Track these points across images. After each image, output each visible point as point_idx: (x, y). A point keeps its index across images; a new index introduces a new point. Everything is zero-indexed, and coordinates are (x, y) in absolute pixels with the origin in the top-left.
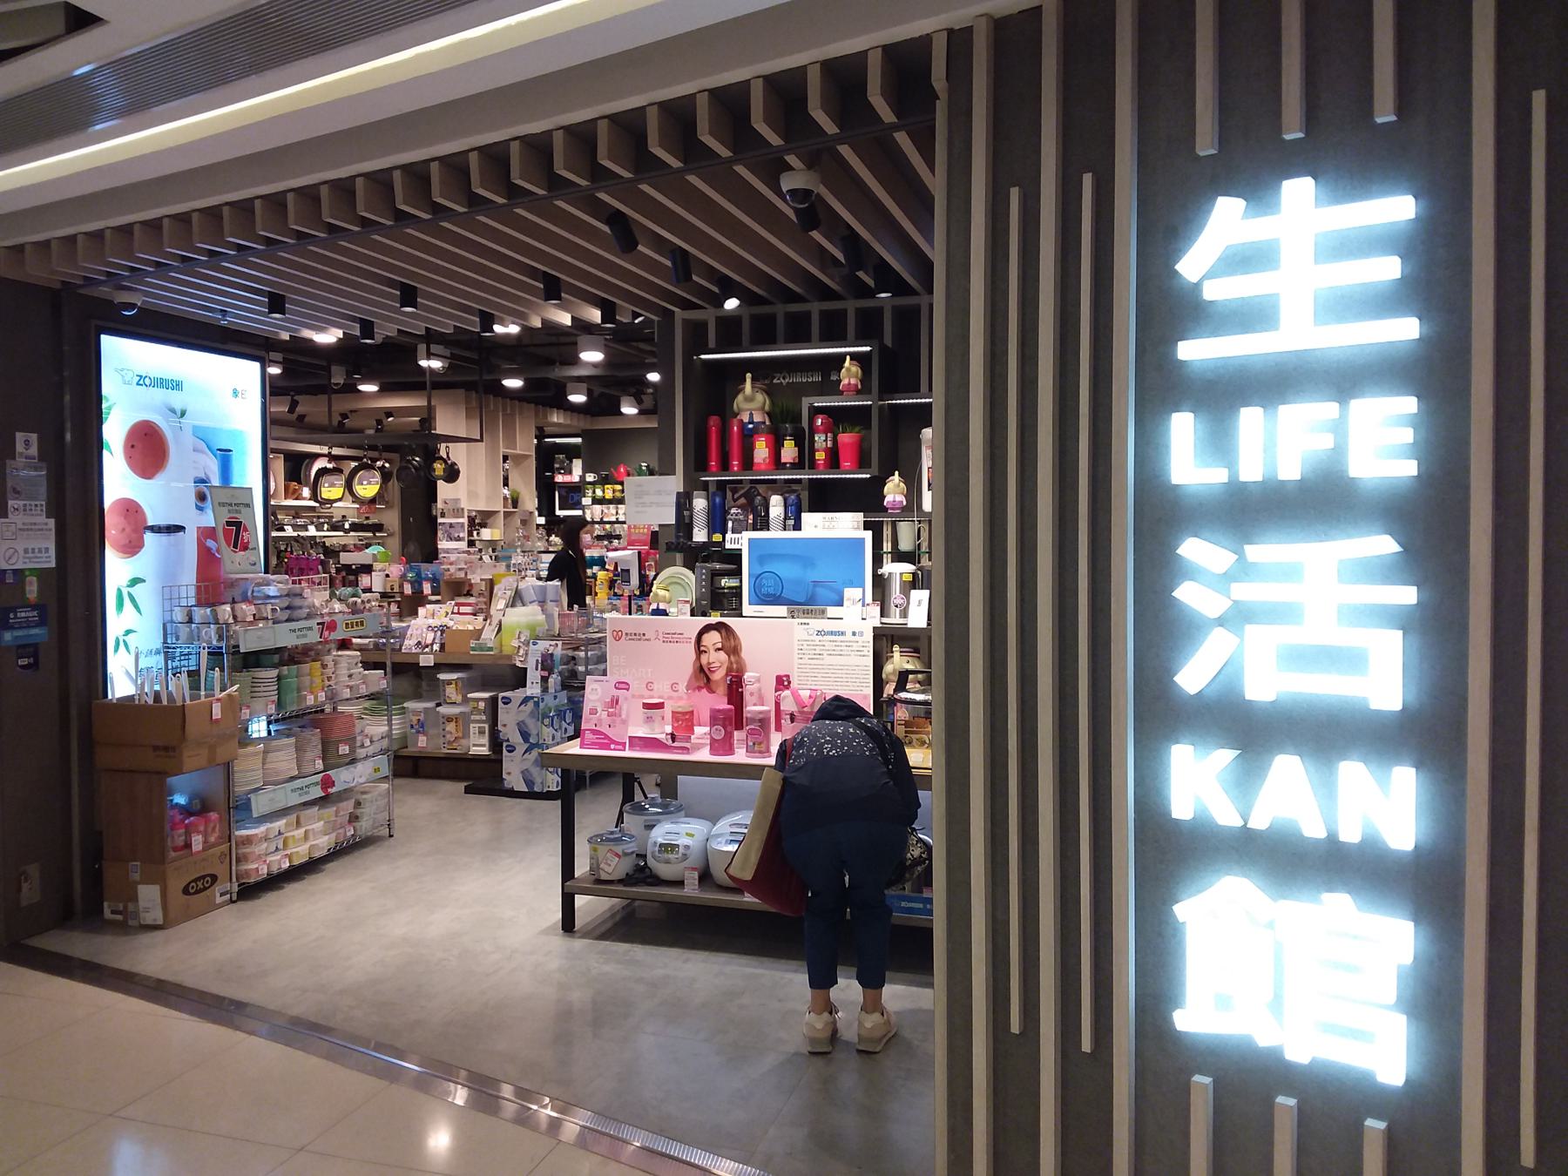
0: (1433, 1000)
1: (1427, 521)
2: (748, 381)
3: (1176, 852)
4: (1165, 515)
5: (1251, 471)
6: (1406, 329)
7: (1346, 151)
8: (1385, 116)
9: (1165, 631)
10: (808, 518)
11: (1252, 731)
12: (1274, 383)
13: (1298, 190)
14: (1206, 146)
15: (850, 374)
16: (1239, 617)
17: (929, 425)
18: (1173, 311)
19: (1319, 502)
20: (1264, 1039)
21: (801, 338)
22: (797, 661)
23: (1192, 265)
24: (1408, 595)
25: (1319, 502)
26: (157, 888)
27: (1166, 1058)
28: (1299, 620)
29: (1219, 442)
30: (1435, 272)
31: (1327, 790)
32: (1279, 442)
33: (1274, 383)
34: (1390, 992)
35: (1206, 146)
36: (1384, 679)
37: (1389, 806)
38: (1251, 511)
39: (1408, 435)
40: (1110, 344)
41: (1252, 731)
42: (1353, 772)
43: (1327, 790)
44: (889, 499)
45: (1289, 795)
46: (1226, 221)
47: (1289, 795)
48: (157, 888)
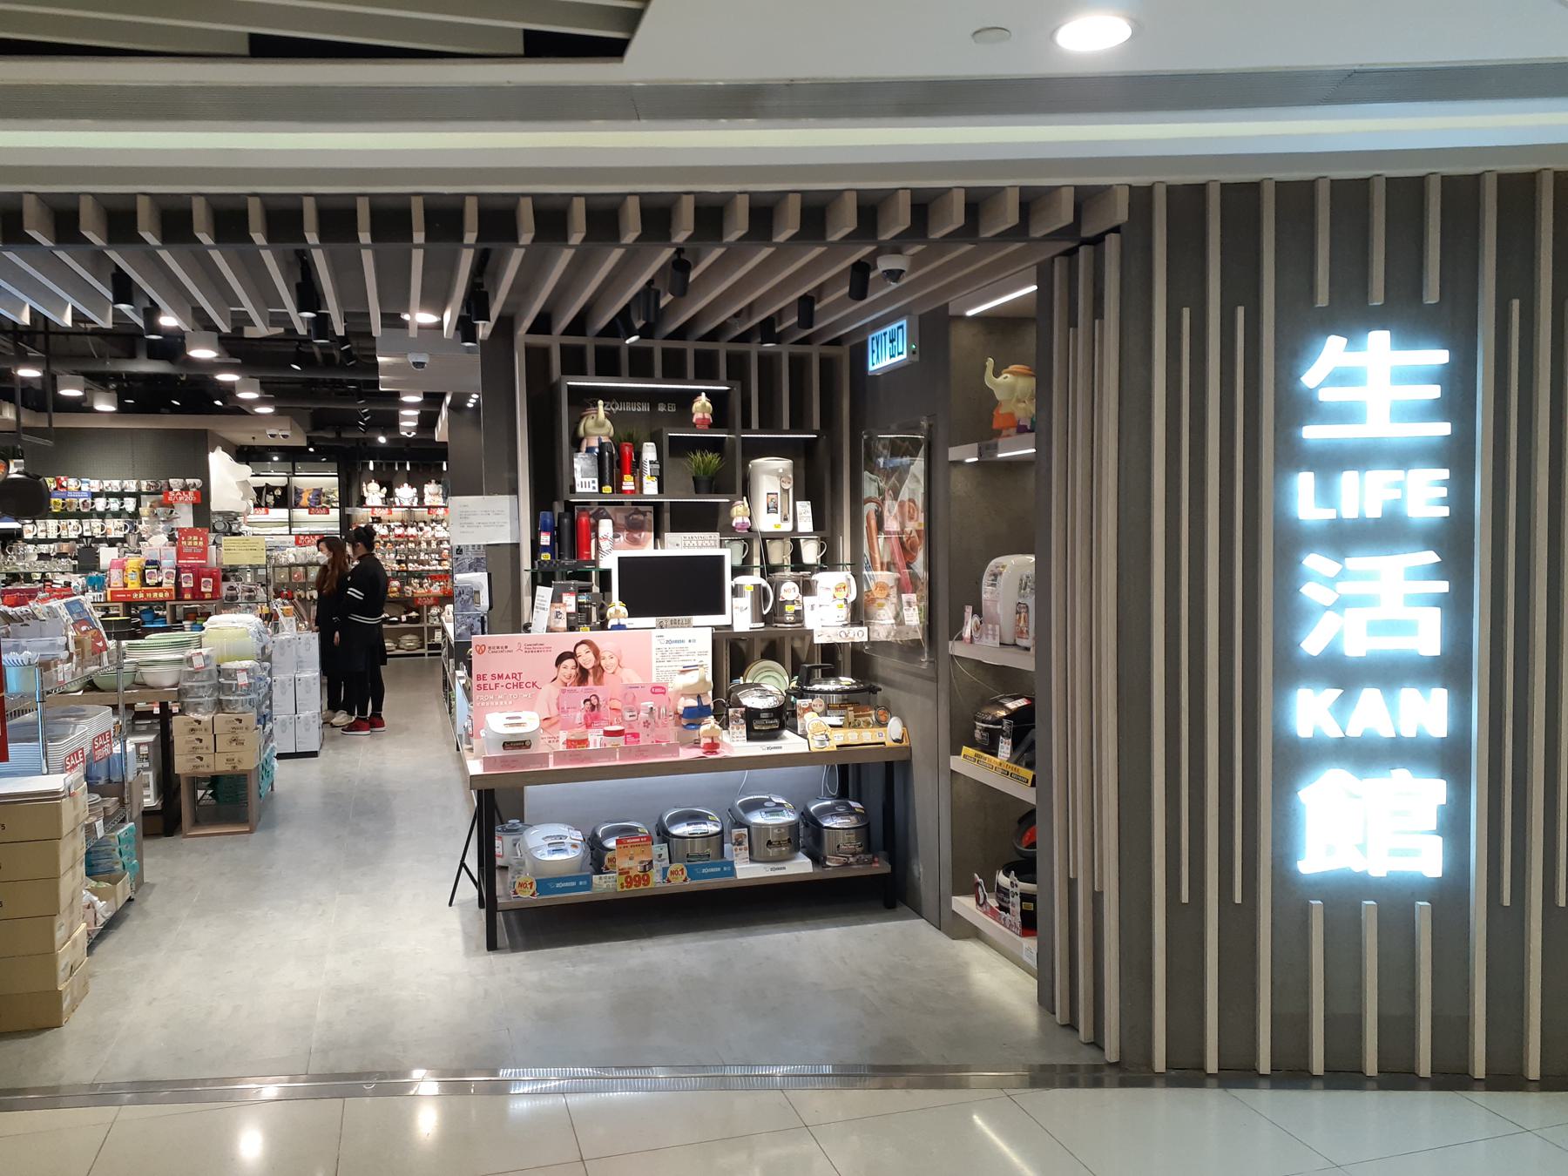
0: (1453, 825)
1: (1451, 541)
2: (601, 408)
3: (1298, 758)
4: (1293, 541)
5: (1349, 512)
6: (1444, 429)
7: (1408, 315)
8: (1432, 296)
9: (1291, 614)
10: (669, 537)
11: (1344, 675)
12: (1362, 457)
13: (1379, 339)
14: (1322, 300)
15: (702, 408)
16: (1341, 605)
17: (123, 409)
18: (1297, 407)
19: (1385, 533)
20: (1358, 867)
21: (647, 374)
22: (654, 664)
23: (1311, 377)
24: (1443, 587)
25: (1385, 533)
27: (1291, 891)
28: (1372, 602)
29: (1326, 494)
31: (1392, 708)
32: (1363, 495)
33: (1362, 457)
34: (1433, 824)
35: (1322, 300)
36: (1428, 639)
37: (1427, 712)
38: (1346, 537)
39: (1443, 492)
40: (1258, 429)
41: (1344, 675)
42: (1409, 695)
43: (1392, 708)
45: (1374, 715)
46: (1332, 352)
47: (1374, 715)
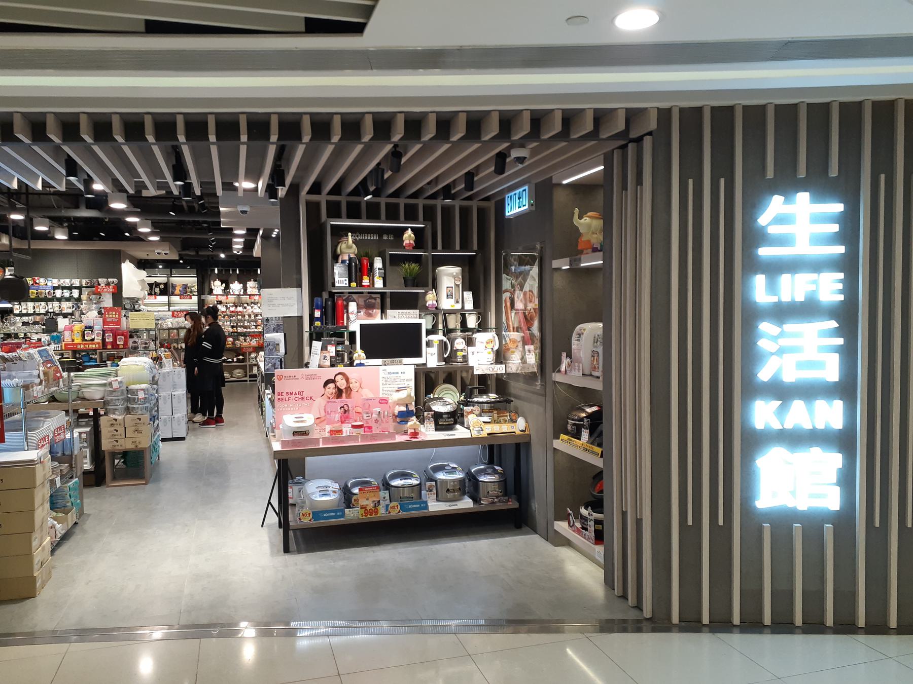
0: (846, 480)
1: (845, 315)
2: (350, 237)
3: (756, 441)
4: (753, 314)
5: (786, 298)
6: (841, 249)
7: (820, 183)
8: (834, 172)
9: (752, 357)
10: (390, 312)
11: (783, 392)
12: (793, 266)
13: (803, 197)
14: (770, 174)
15: (408, 237)
16: (781, 352)
17: (71, 238)
18: (755, 237)
19: (807, 310)
20: (790, 504)
21: (377, 218)
22: (381, 386)
23: (763, 219)
24: (840, 341)
25: (807, 310)
26: (308, 459)
27: (752, 518)
28: (799, 350)
29: (772, 287)
30: (848, 232)
31: (811, 412)
32: (794, 288)
33: (793, 266)
34: (834, 479)
35: (770, 174)
36: (831, 371)
37: (831, 414)
38: (784, 313)
39: (840, 286)
40: (733, 249)
41: (783, 392)
42: (820, 404)
43: (811, 412)
44: (406, 242)
45: (800, 416)
46: (776, 205)
47: (800, 416)
48: (308, 459)
